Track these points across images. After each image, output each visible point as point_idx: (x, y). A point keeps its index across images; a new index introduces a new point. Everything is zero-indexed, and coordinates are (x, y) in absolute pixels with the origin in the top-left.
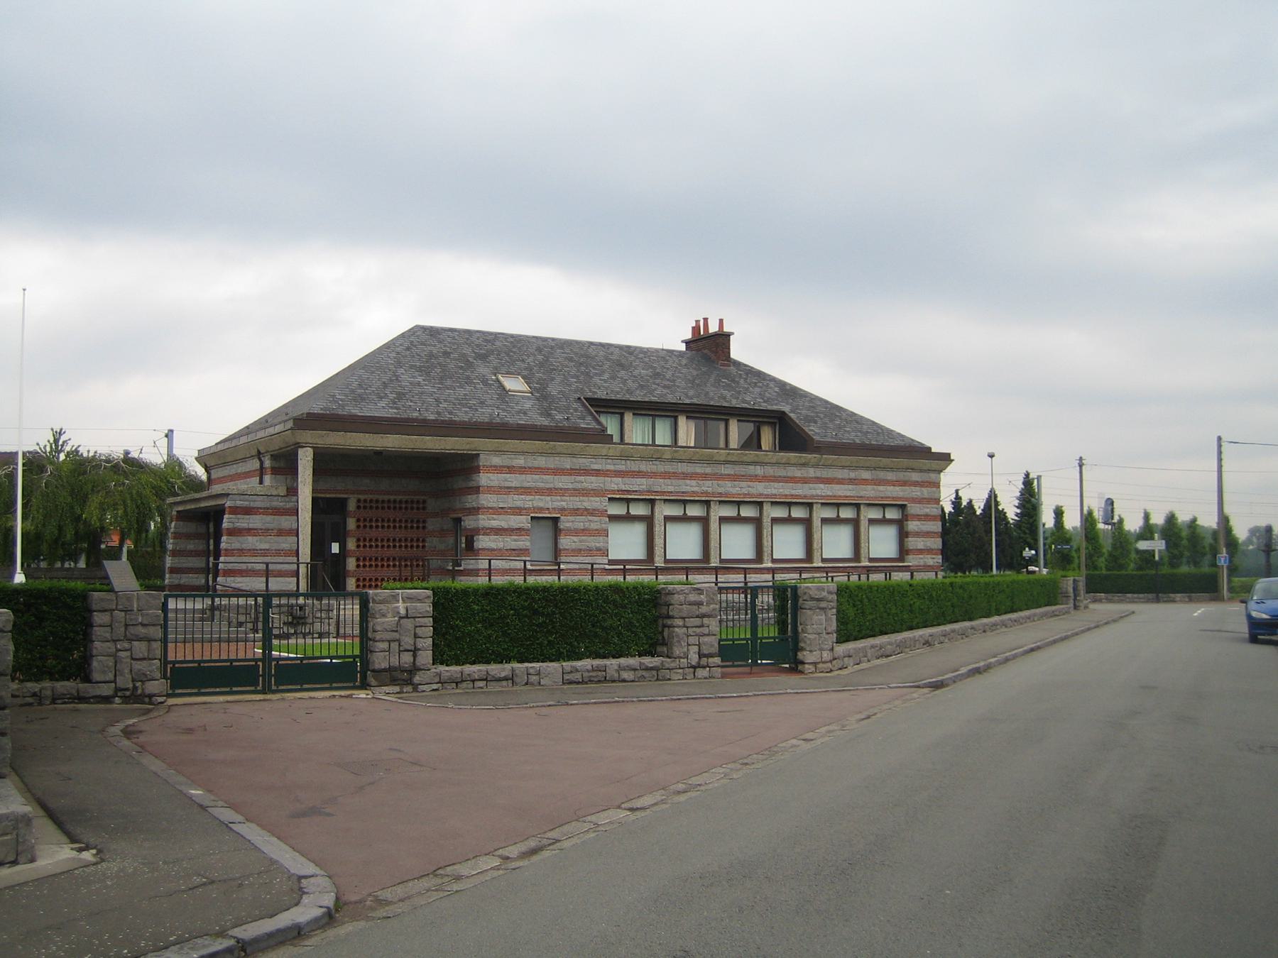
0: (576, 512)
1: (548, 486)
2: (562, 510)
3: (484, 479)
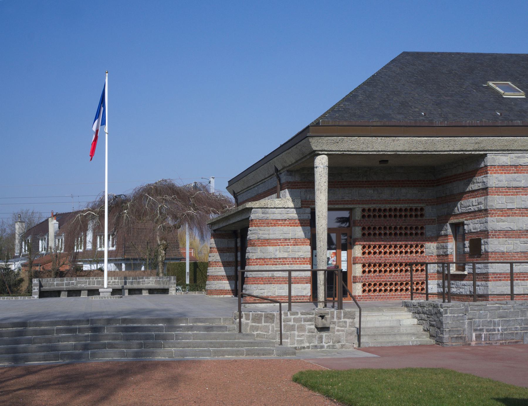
3: (493, 180)
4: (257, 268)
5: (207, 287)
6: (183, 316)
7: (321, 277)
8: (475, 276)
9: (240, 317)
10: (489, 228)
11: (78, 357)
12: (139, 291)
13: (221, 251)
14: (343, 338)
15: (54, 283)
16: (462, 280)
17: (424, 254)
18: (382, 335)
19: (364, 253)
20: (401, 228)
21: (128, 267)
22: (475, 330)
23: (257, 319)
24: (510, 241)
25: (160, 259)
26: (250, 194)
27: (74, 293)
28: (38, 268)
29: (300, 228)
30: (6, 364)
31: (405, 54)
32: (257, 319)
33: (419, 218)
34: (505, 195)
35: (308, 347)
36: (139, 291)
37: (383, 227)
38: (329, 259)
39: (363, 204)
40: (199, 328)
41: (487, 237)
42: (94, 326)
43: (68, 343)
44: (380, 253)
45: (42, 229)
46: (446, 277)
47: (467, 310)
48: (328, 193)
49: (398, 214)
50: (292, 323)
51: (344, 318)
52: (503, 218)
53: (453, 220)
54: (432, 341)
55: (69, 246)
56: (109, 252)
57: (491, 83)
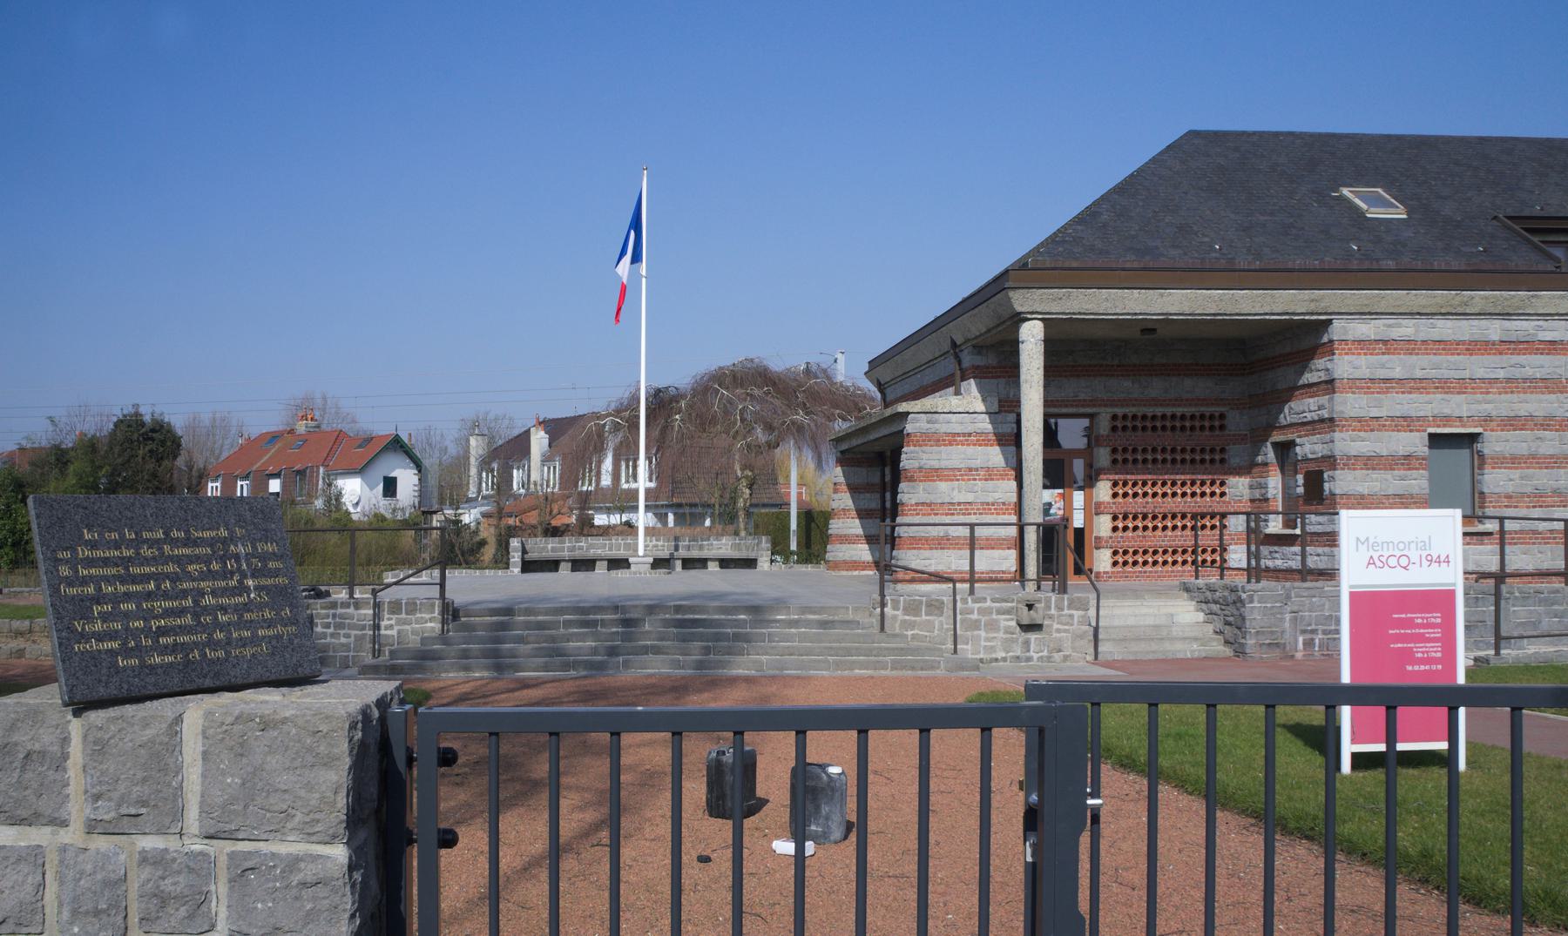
0: (1513, 423)
2: (1488, 419)
3: (1343, 366)
4: (917, 520)
5: (829, 556)
6: (780, 604)
7: (1031, 537)
8: (1304, 540)
9: (883, 605)
10: (1337, 453)
11: (599, 667)
12: (702, 563)
13: (854, 489)
14: (1067, 645)
15: (545, 547)
16: (1292, 545)
17: (1227, 498)
18: (1138, 639)
19: (1115, 495)
20: (1183, 451)
21: (680, 519)
22: (1304, 632)
23: (912, 608)
24: (1375, 475)
25: (741, 503)
26: (907, 387)
27: (583, 564)
28: (511, 521)
29: (997, 449)
30: (486, 674)
31: (1193, 134)
32: (912, 608)
35: (1004, 659)
36: (702, 563)
38: (1050, 505)
40: (808, 624)
41: (1333, 467)
42: (627, 618)
43: (582, 644)
44: (1145, 494)
45: (518, 447)
46: (1258, 539)
47: (1288, 597)
48: (1046, 386)
49: (1178, 424)
50: (975, 616)
51: (1069, 608)
52: (1362, 434)
53: (1278, 437)
54: (1228, 652)
55: (570, 479)
56: (648, 491)
57: (1346, 191)
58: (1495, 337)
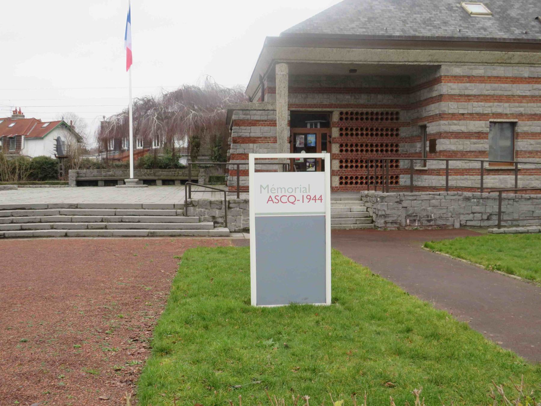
1: (506, 93)
2: (520, 115)
3: (444, 88)
33: (395, 121)
34: (457, 102)
37: (360, 129)
39: (340, 107)
53: (421, 124)
58: (526, 75)
